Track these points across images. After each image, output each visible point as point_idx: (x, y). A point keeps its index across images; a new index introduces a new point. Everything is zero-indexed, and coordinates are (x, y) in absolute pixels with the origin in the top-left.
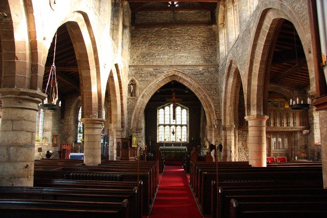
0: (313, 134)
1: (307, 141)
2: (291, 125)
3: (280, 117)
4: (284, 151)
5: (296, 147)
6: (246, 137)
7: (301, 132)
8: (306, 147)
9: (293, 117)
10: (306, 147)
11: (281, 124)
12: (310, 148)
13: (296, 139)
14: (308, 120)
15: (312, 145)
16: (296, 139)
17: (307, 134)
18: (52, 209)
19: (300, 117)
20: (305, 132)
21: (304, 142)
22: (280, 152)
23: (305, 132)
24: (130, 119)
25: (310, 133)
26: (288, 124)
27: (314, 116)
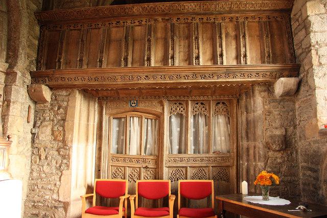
0: (312, 89)
1: (290, 122)
2: (204, 60)
3: (188, 37)
4: (209, 159)
5: (252, 144)
6: (66, 109)
7: (268, 86)
8: (286, 144)
9: (237, 38)
10: (286, 144)
11: (215, 57)
12: (301, 145)
13: (251, 116)
14: (291, 43)
15: (308, 133)
16: (251, 116)
17: (291, 95)
18: (210, 81)
19: (261, 37)
20: (282, 85)
21: (282, 126)
22: (198, 164)
23: (282, 85)
24: (127, 51)
25: (302, 88)
26: (215, 57)
27: (312, 19)
